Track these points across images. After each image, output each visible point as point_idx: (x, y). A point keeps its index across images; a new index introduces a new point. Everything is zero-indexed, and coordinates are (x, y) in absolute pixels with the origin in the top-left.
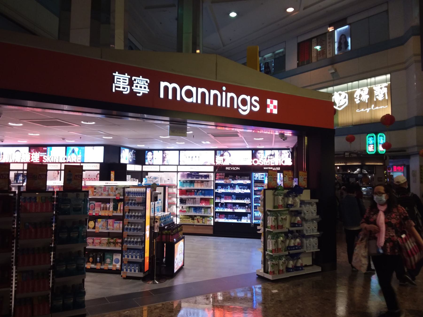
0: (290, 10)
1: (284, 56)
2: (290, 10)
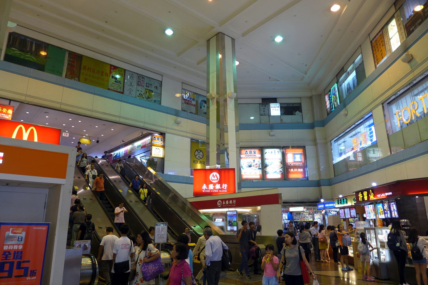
0: (252, 118)
1: (363, 62)
2: (252, 118)
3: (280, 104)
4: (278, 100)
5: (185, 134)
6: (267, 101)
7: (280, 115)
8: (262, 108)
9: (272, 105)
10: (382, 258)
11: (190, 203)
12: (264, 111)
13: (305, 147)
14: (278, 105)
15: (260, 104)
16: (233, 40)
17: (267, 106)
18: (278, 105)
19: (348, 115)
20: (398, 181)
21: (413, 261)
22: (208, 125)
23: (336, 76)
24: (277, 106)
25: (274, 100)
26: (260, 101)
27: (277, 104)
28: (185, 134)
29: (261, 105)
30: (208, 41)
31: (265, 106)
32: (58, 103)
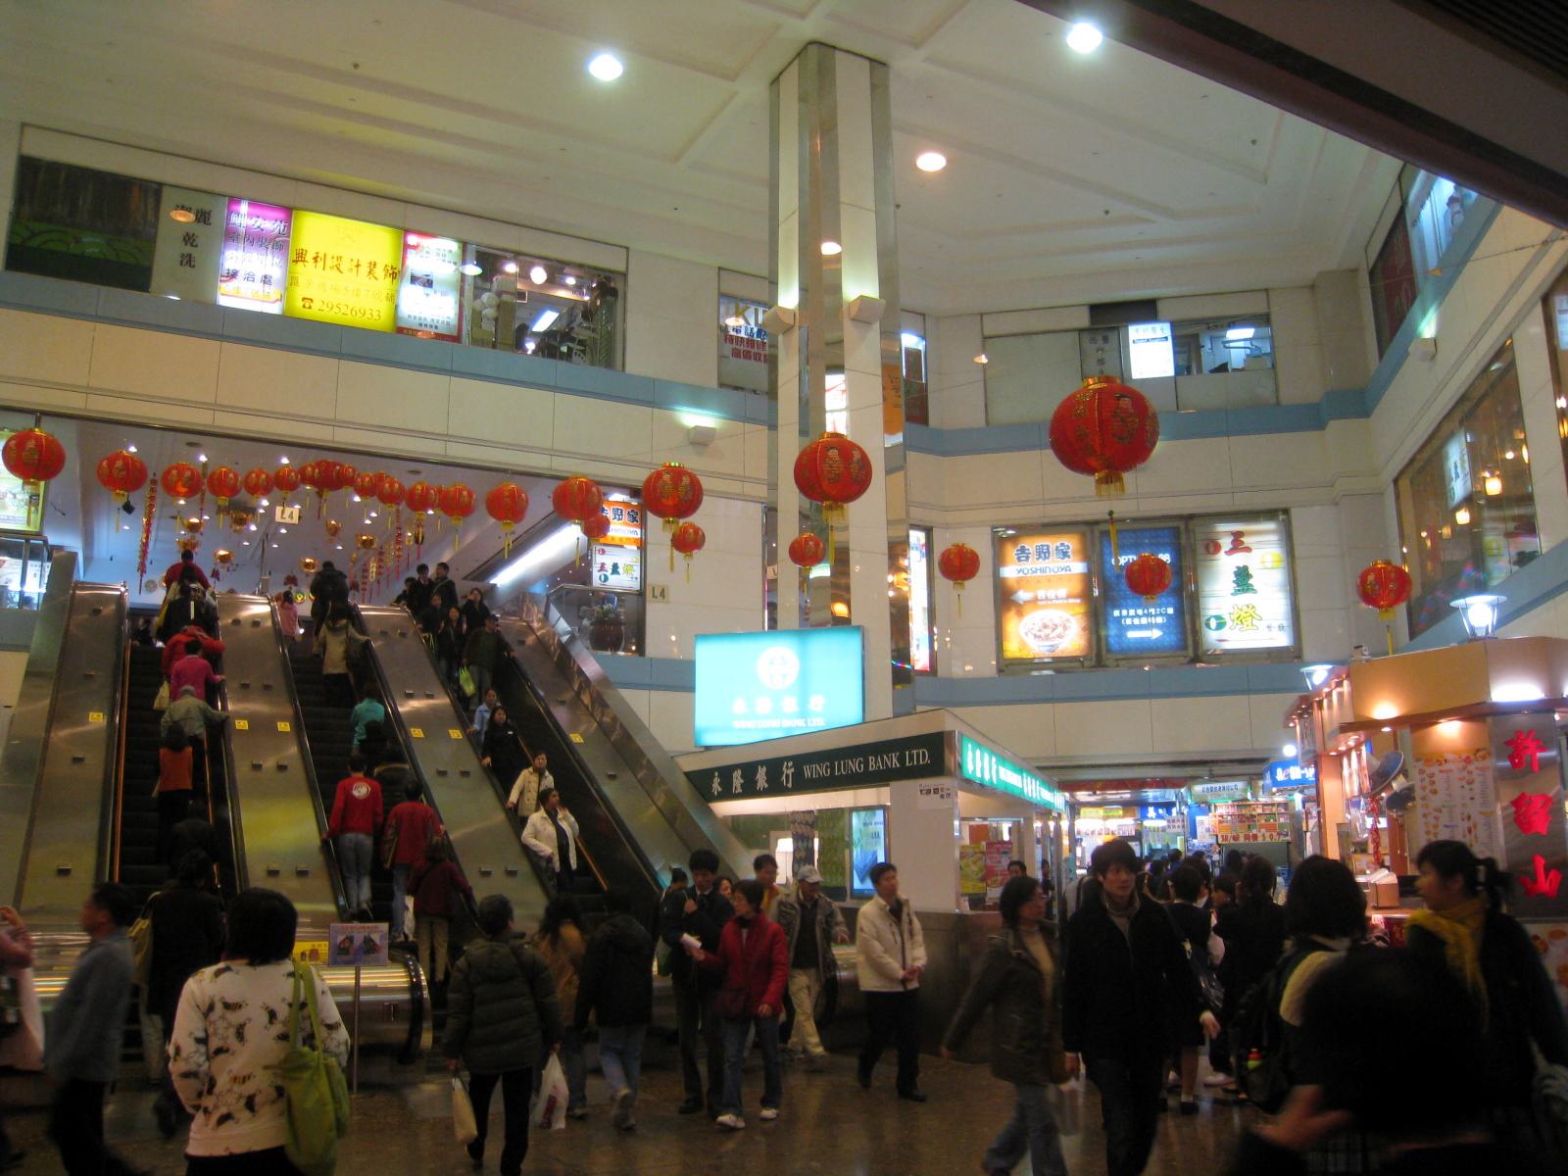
3: (1174, 326)
4: (1160, 306)
5: (735, 487)
6: (1112, 317)
7: (1170, 372)
8: (1090, 347)
9: (1136, 332)
10: (594, 662)
11: (687, 774)
12: (1101, 362)
13: (1286, 511)
14: (1163, 329)
15: (1081, 331)
16: (877, 64)
17: (1112, 336)
18: (1163, 329)
19: (1439, 356)
20: (865, 490)
21: (1365, 868)
22: (773, 426)
23: (1399, 178)
24: (1159, 334)
25: (1146, 310)
26: (1083, 319)
27: (1158, 326)
28: (735, 487)
29: (1086, 337)
30: (776, 81)
31: (1106, 340)
32: (542, 451)
